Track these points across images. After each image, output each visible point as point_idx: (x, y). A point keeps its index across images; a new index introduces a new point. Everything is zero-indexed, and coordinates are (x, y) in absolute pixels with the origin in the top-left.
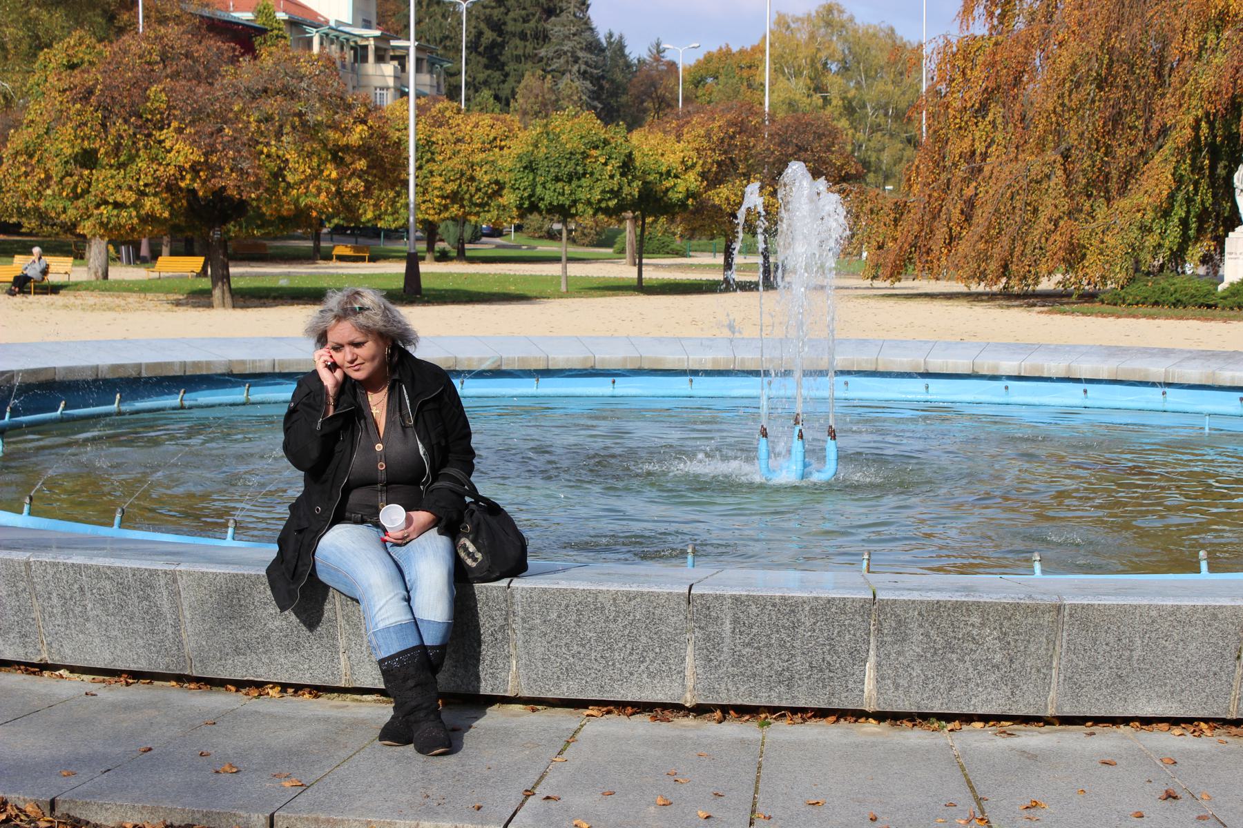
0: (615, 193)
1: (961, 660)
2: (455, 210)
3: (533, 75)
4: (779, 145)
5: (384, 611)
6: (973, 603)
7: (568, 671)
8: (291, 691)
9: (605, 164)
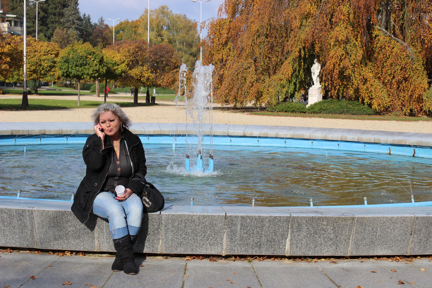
0: (98, 71)
1: (320, 237)
2: (34, 75)
3: (60, 28)
4: (154, 55)
5: (118, 222)
6: (325, 217)
7: (180, 244)
8: (74, 253)
9: (94, 61)
